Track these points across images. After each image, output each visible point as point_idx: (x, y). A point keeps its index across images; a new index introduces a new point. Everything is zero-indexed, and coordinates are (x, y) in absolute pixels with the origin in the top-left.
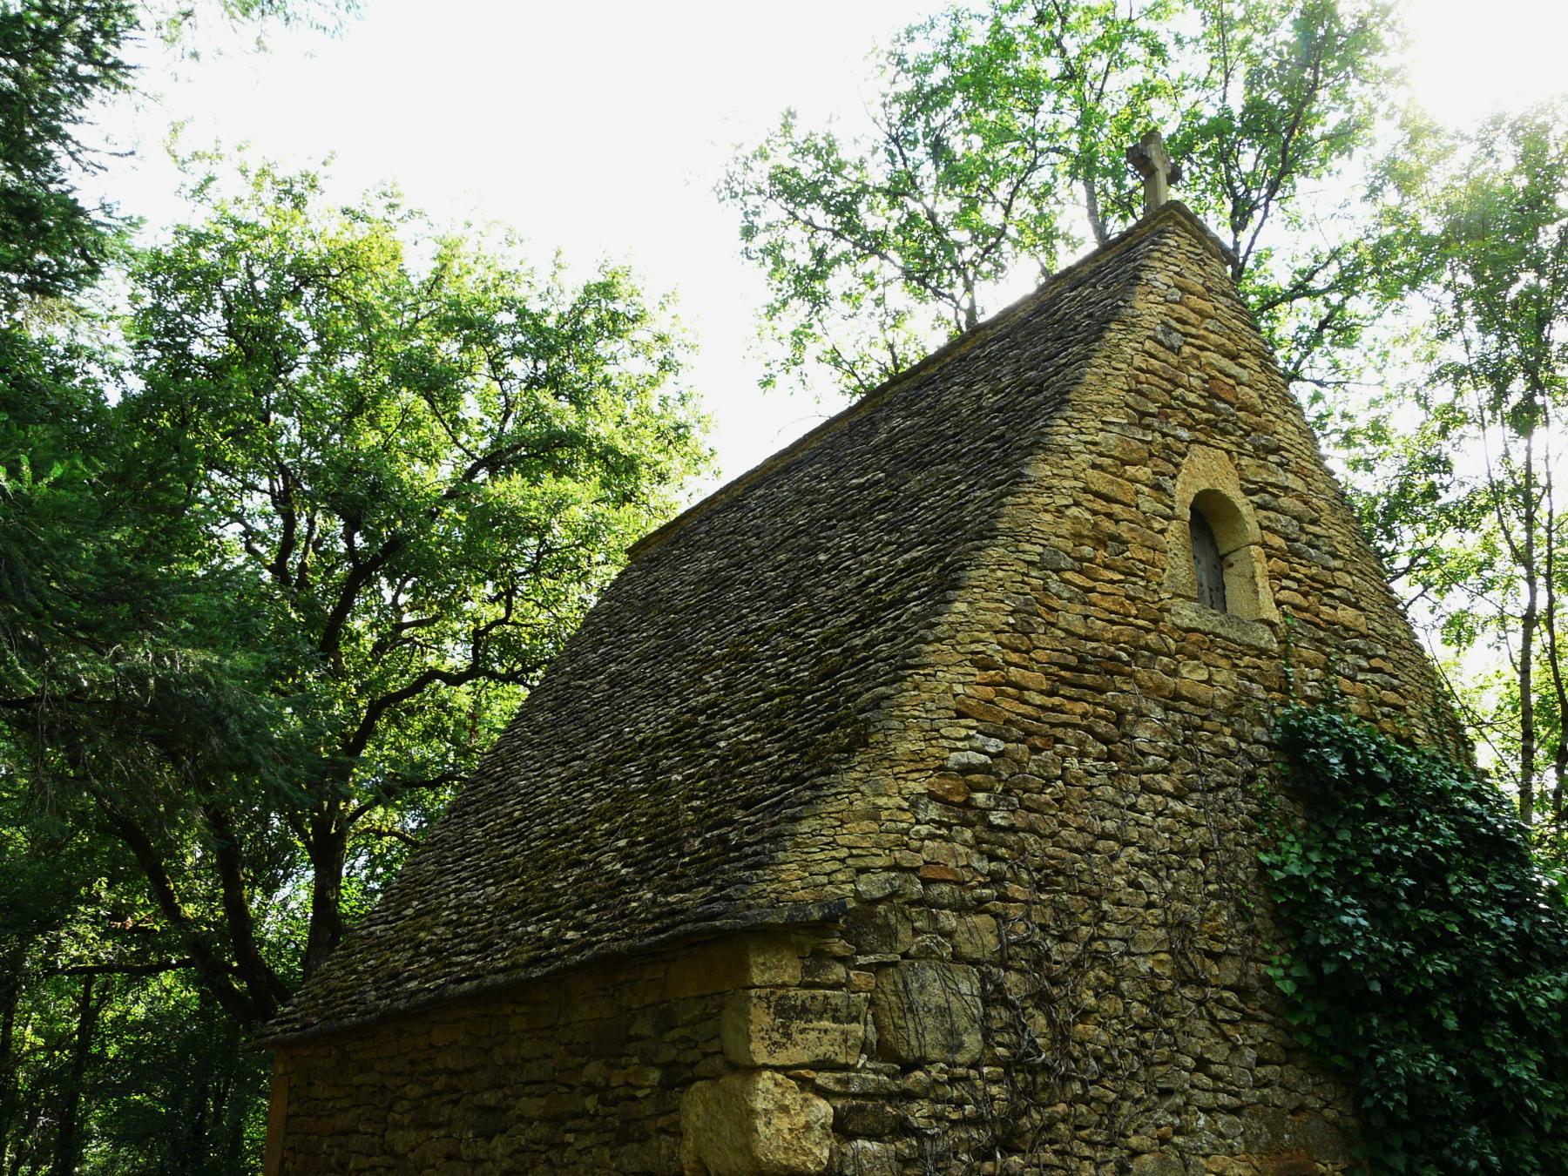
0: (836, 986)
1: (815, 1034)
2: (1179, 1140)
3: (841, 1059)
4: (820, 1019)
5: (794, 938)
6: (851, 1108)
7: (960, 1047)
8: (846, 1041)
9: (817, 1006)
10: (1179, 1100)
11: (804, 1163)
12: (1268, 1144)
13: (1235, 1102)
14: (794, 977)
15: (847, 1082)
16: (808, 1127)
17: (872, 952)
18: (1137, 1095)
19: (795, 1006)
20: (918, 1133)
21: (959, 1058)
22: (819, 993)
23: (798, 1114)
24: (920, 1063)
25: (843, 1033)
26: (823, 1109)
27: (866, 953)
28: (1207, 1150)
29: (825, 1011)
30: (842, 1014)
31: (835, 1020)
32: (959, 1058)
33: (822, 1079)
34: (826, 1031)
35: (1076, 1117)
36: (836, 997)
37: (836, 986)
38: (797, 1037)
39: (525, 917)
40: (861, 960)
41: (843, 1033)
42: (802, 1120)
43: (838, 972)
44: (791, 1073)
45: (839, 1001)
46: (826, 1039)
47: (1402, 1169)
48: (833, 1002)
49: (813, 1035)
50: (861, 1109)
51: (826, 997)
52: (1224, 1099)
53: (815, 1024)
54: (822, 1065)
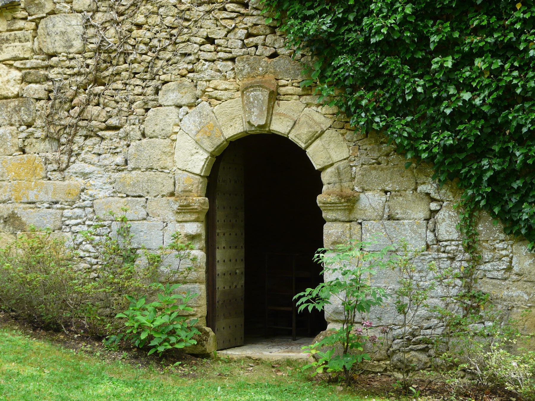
0: (21, 29)
1: (12, 48)
2: (191, 75)
3: (21, 56)
4: (14, 42)
5: (4, 14)
6: (26, 73)
7: (71, 46)
8: (23, 49)
9: (12, 38)
10: (192, 58)
11: (7, 93)
12: (249, 73)
13: (230, 55)
14: (4, 28)
15: (25, 64)
16: (8, 81)
17: (34, 15)
18: (167, 57)
19: (3, 39)
20: (51, 80)
21: (71, 50)
22: (13, 33)
23: (5, 77)
24: (54, 55)
25: (22, 46)
26: (18, 74)
27: (31, 16)
28: (208, 78)
29: (15, 39)
30: (23, 39)
31: (20, 41)
32: (71, 50)
33: (17, 64)
34: (16, 46)
35: (132, 69)
36: (19, 33)
37: (21, 29)
38: (4, 49)
39: (298, 29)
40: (29, 18)
41: (22, 46)
42: (6, 79)
43: (21, 24)
44: (4, 63)
45: (20, 35)
46: (15, 49)
47: (462, 82)
48: (18, 35)
49: (10, 48)
50: (29, 73)
51: (15, 34)
52: (221, 55)
53: (13, 44)
54: (15, 59)
